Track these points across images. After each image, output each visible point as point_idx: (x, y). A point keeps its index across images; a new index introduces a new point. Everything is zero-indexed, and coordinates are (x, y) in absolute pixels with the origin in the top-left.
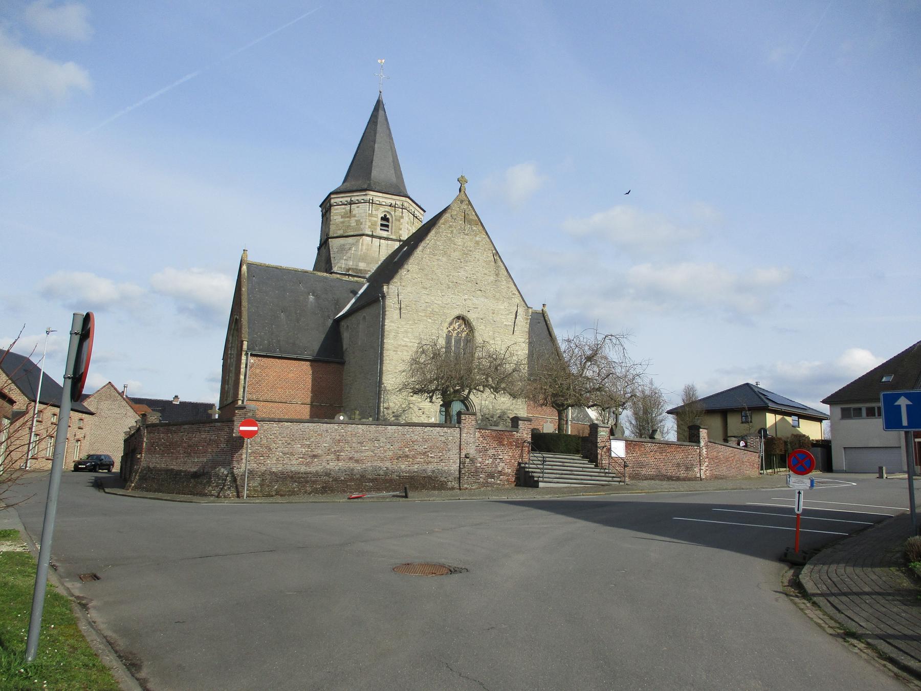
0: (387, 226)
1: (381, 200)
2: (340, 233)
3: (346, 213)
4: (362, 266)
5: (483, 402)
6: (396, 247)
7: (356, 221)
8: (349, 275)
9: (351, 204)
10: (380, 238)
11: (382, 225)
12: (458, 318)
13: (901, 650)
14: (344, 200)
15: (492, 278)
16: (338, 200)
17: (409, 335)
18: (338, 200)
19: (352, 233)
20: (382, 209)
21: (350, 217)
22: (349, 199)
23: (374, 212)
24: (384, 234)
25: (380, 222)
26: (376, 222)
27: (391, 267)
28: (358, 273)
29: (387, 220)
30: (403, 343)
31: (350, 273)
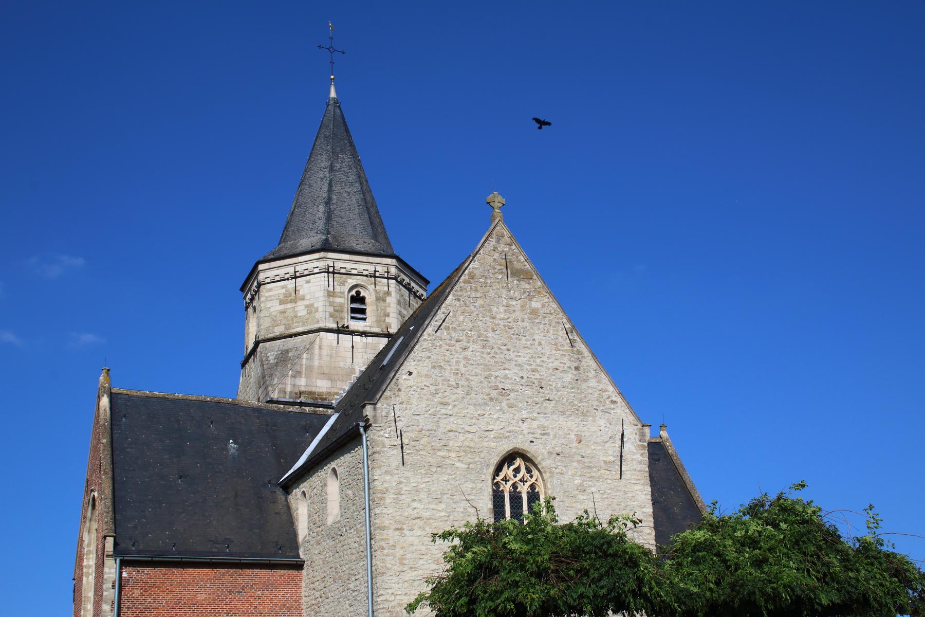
0: (363, 311)
1: (348, 266)
2: (278, 330)
3: (287, 295)
4: (322, 386)
5: (539, 559)
6: (381, 347)
7: (307, 306)
8: (301, 404)
9: (296, 278)
10: (353, 333)
11: (353, 310)
12: (510, 458)
13: (291, 336)
14: (281, 272)
15: (569, 377)
16: (271, 274)
17: (423, 495)
18: (271, 274)
19: (301, 329)
20: (352, 281)
21: (294, 301)
22: (291, 270)
23: (338, 289)
24: (355, 325)
25: (348, 306)
26: (341, 305)
27: (375, 380)
28: (319, 402)
29: (362, 300)
30: (414, 514)
31: (303, 399)
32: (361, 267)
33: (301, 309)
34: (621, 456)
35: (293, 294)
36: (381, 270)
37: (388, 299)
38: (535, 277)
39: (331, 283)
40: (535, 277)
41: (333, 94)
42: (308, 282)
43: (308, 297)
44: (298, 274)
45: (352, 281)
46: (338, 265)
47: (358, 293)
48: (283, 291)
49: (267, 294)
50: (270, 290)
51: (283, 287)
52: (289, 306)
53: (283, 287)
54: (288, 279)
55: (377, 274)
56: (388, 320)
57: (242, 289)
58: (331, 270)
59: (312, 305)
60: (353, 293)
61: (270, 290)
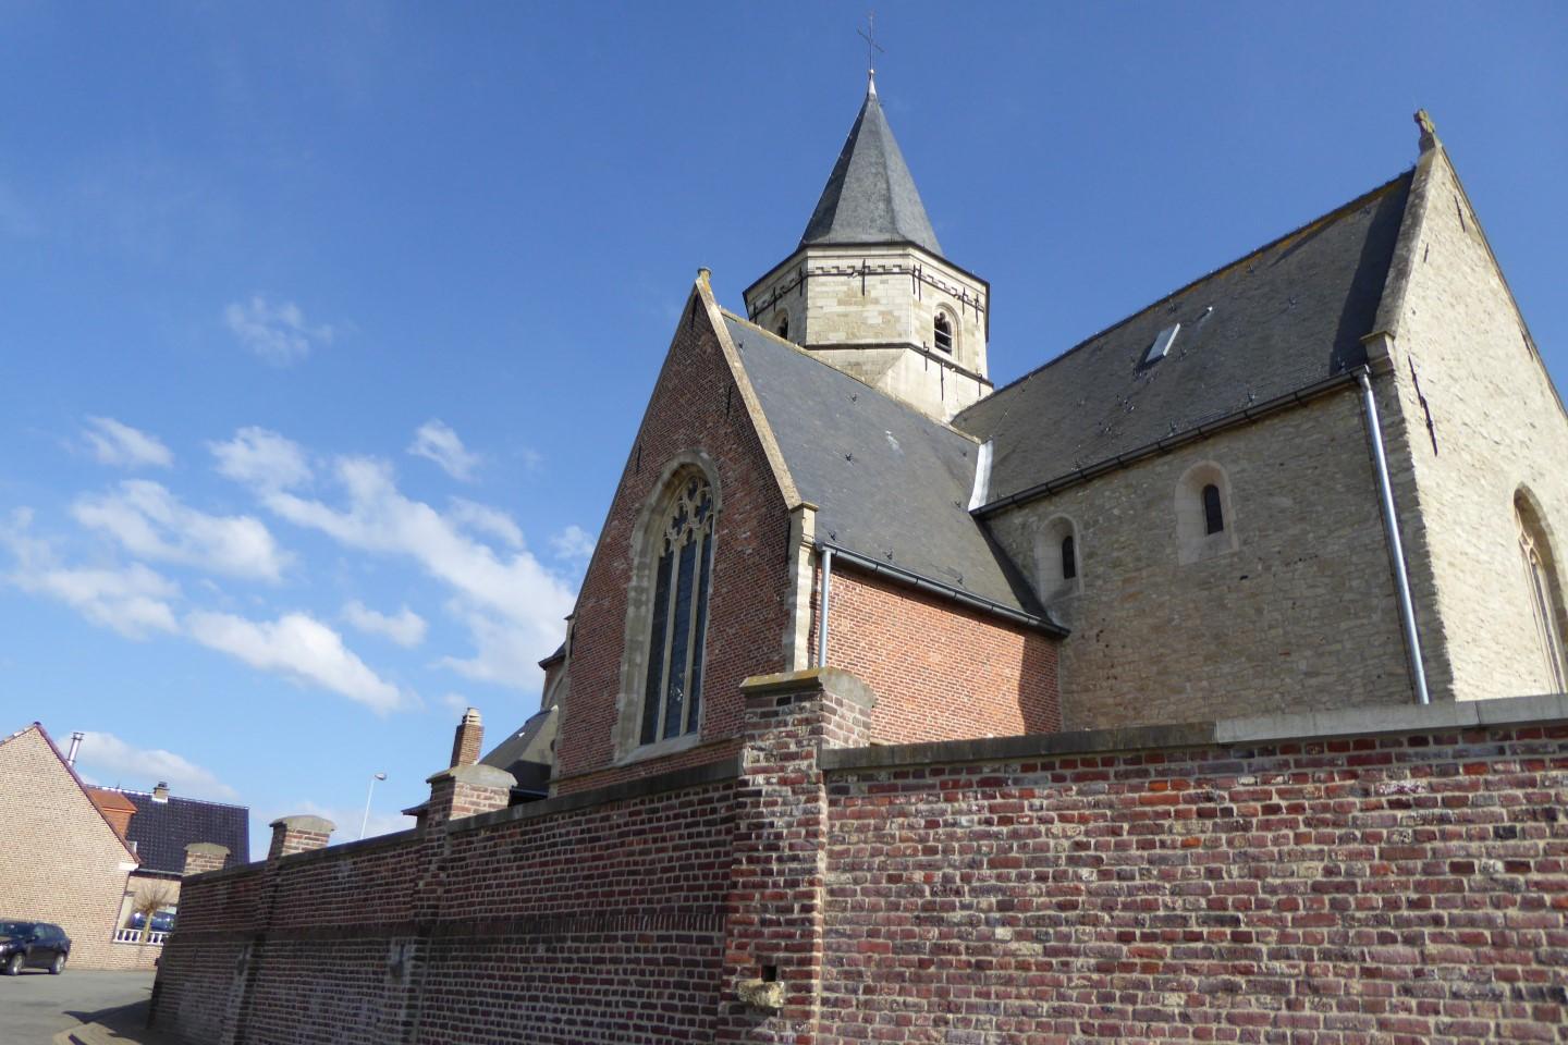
1: (938, 277)
7: (882, 313)
16: (828, 264)
18: (828, 264)
22: (858, 263)
33: (872, 315)
34: (1429, 425)
35: (860, 294)
36: (971, 295)
41: (873, 90)
42: (882, 282)
43: (884, 301)
48: (845, 288)
49: (818, 289)
50: (823, 284)
51: (843, 284)
52: (853, 309)
53: (843, 284)
59: (890, 313)
61: (823, 284)
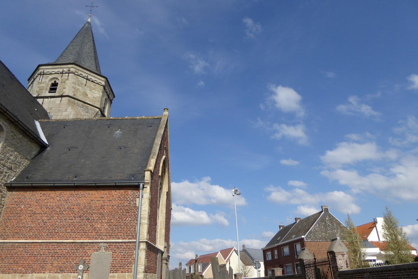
1: (50, 71)
20: (51, 77)
32: (56, 70)
37: (67, 82)
38: (415, 262)
39: (41, 79)
40: (415, 262)
44: (64, 72)
45: (51, 77)
46: (46, 71)
47: (55, 81)
54: (58, 73)
55: (64, 72)
56: (64, 90)
57: (29, 80)
58: (42, 73)
60: (53, 82)
